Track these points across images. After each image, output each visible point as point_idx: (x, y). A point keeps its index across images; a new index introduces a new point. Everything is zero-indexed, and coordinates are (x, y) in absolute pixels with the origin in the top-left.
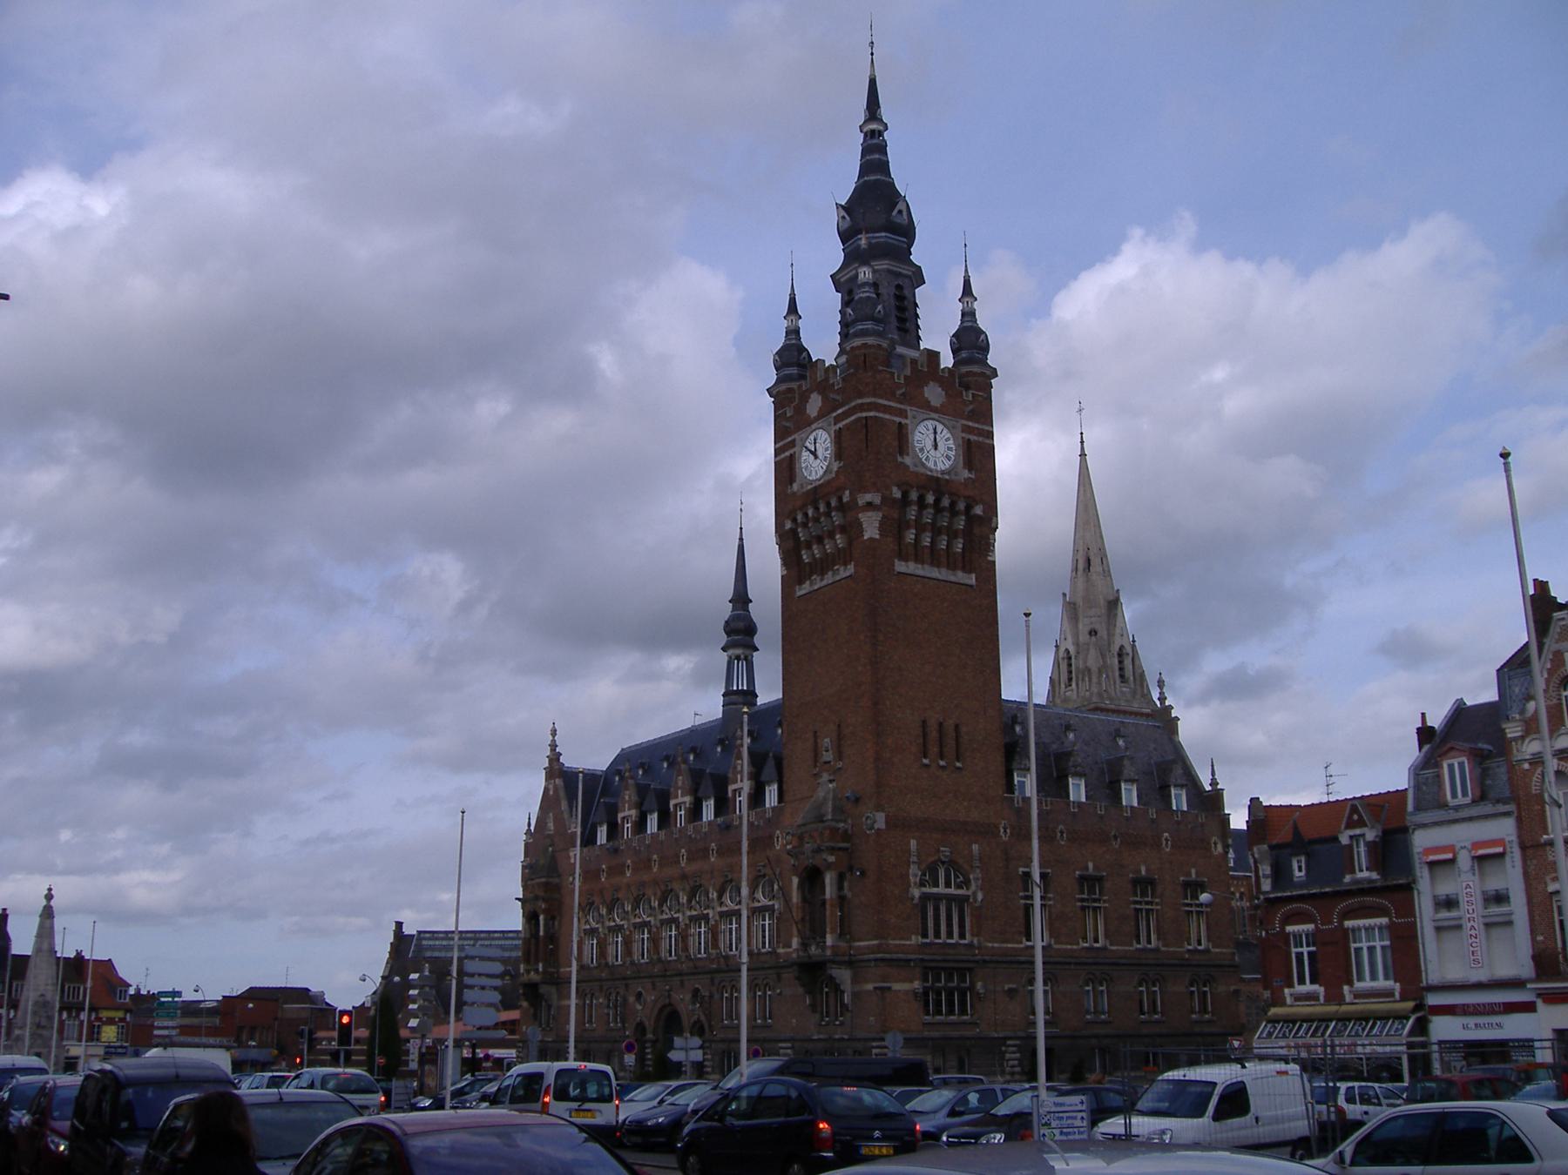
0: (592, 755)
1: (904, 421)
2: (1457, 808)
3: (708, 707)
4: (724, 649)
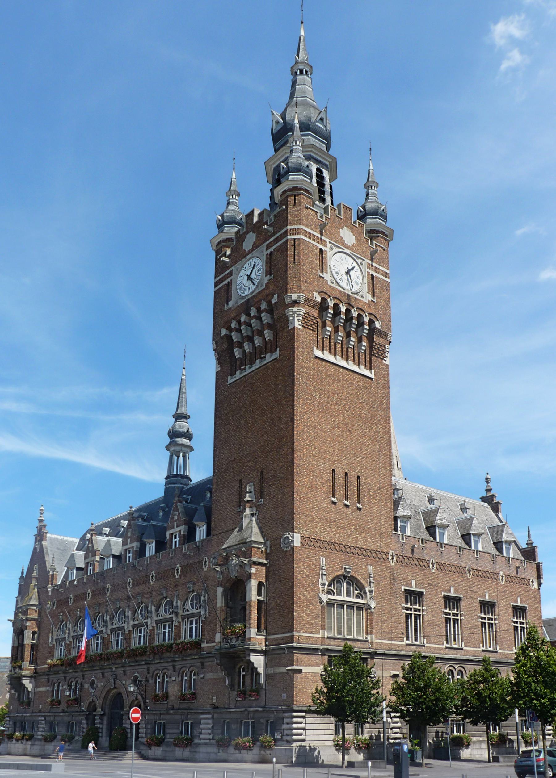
1: (324, 248)
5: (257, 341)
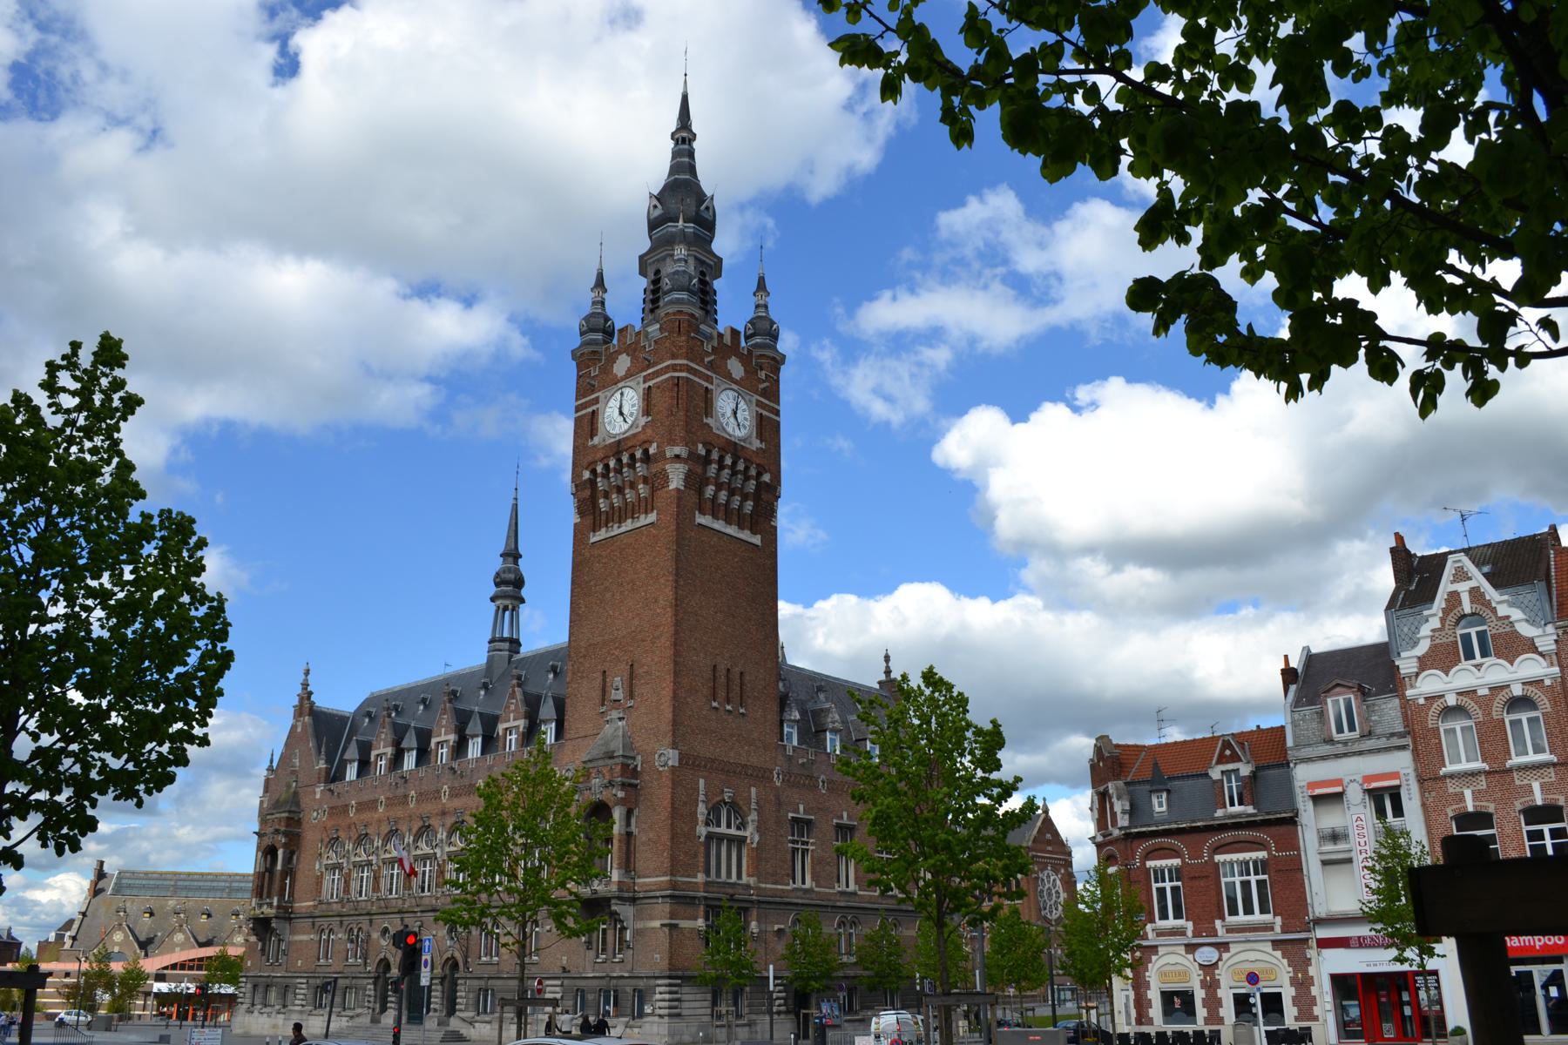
0: (341, 697)
2: (1345, 743)
3: (472, 655)
4: (493, 599)
5: (630, 495)
